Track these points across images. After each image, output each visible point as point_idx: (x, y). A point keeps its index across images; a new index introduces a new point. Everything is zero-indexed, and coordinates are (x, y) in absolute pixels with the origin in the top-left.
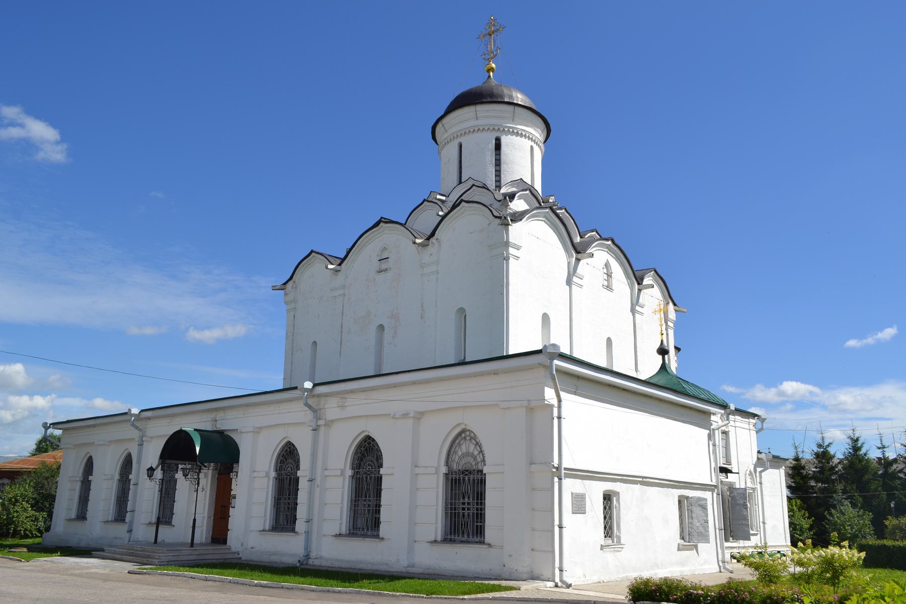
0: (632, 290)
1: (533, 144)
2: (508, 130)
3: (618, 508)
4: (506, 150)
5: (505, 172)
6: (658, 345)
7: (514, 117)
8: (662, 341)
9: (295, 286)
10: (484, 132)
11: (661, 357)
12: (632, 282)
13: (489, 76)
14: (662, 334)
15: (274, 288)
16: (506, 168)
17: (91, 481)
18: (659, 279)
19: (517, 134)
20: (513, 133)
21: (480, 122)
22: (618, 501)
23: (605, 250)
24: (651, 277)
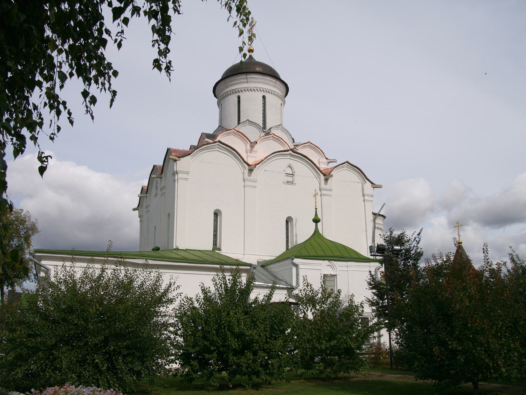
1: (263, 94)
15: (134, 210)
18: (379, 186)
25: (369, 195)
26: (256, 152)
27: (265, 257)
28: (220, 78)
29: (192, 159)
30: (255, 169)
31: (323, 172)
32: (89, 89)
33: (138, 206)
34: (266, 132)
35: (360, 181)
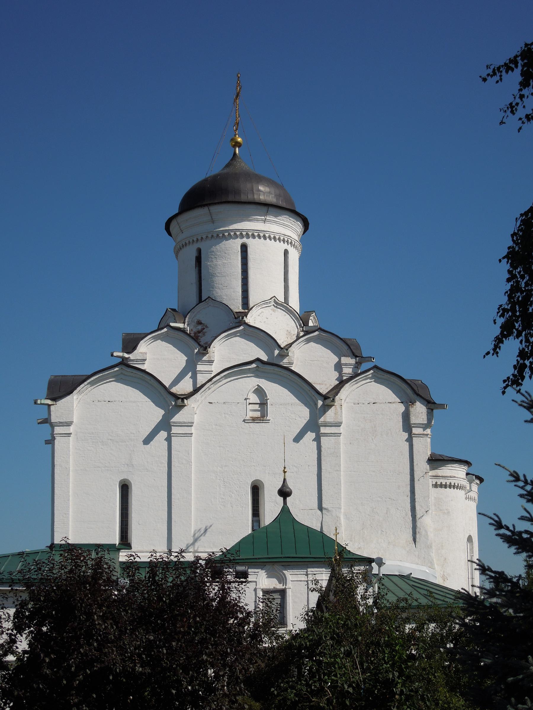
6: (279, 485)
13: (235, 154)
26: (211, 362)
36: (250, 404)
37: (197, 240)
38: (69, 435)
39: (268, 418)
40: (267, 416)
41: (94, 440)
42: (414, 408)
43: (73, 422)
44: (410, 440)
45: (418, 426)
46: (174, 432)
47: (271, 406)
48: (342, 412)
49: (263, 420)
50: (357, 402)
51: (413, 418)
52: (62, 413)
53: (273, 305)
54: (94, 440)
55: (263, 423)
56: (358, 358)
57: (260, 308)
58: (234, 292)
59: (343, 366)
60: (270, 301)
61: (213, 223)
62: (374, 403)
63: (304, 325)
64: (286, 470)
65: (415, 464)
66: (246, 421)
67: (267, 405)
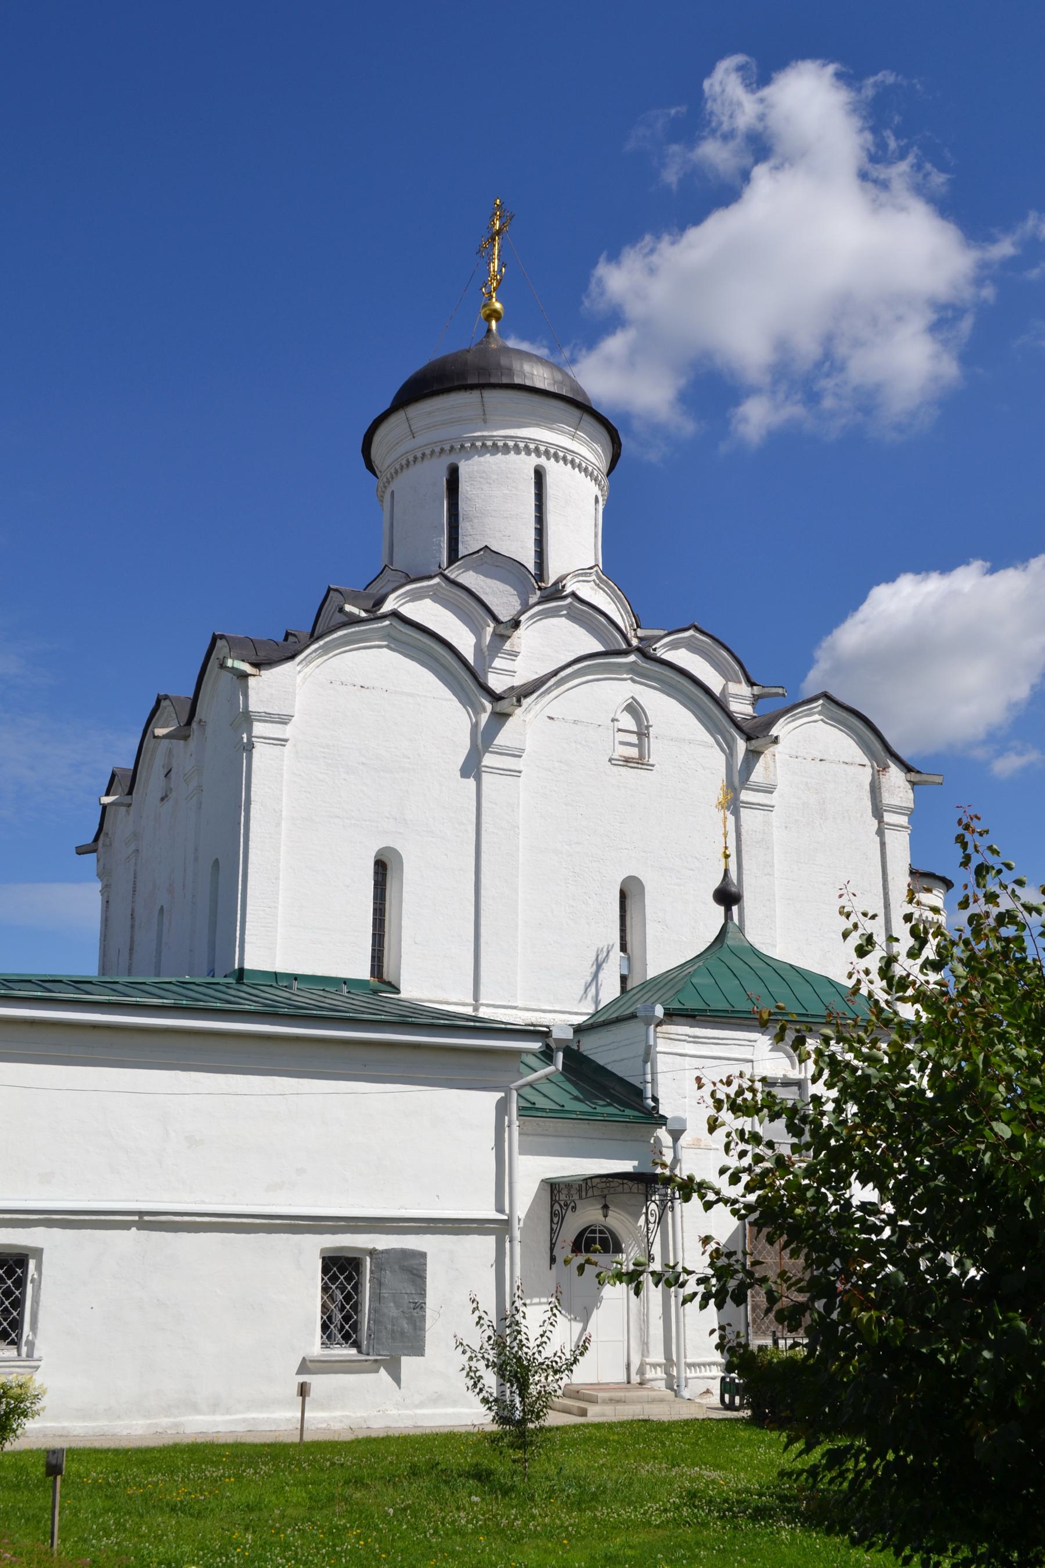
0: (730, 755)
1: (533, 461)
2: (484, 445)
3: (36, 1283)
4: (468, 489)
5: (466, 538)
6: (716, 882)
7: (484, 414)
8: (726, 871)
9: (108, 843)
10: (426, 462)
11: (722, 909)
12: (729, 738)
13: (489, 330)
14: (727, 856)
15: (81, 851)
16: (469, 528)
17: (788, 1133)
18: (845, 714)
19: (495, 449)
20: (485, 449)
21: (421, 439)
22: (39, 1268)
23: (625, 676)
24: (820, 713)
25: (901, 808)
26: (514, 654)
27: (542, 1015)
28: (387, 406)
29: (302, 674)
30: (518, 711)
31: (744, 725)
32: (725, 818)
33: (96, 839)
34: (547, 592)
35: (866, 761)
36: (619, 730)
37: (452, 448)
38: (283, 741)
39: (651, 762)
40: (649, 757)
41: (330, 762)
42: (887, 777)
43: (293, 716)
44: (880, 833)
45: (897, 810)
46: (488, 765)
47: (656, 740)
48: (775, 767)
49: (642, 764)
50: (794, 753)
51: (886, 794)
52: (272, 694)
53: (594, 581)
54: (330, 762)
55: (641, 769)
56: (755, 687)
57: (576, 580)
58: (522, 548)
59: (730, 699)
60: (591, 571)
61: (485, 422)
62: (821, 760)
63: (638, 626)
64: (728, 853)
65: (890, 878)
66: (613, 762)
67: (648, 737)
